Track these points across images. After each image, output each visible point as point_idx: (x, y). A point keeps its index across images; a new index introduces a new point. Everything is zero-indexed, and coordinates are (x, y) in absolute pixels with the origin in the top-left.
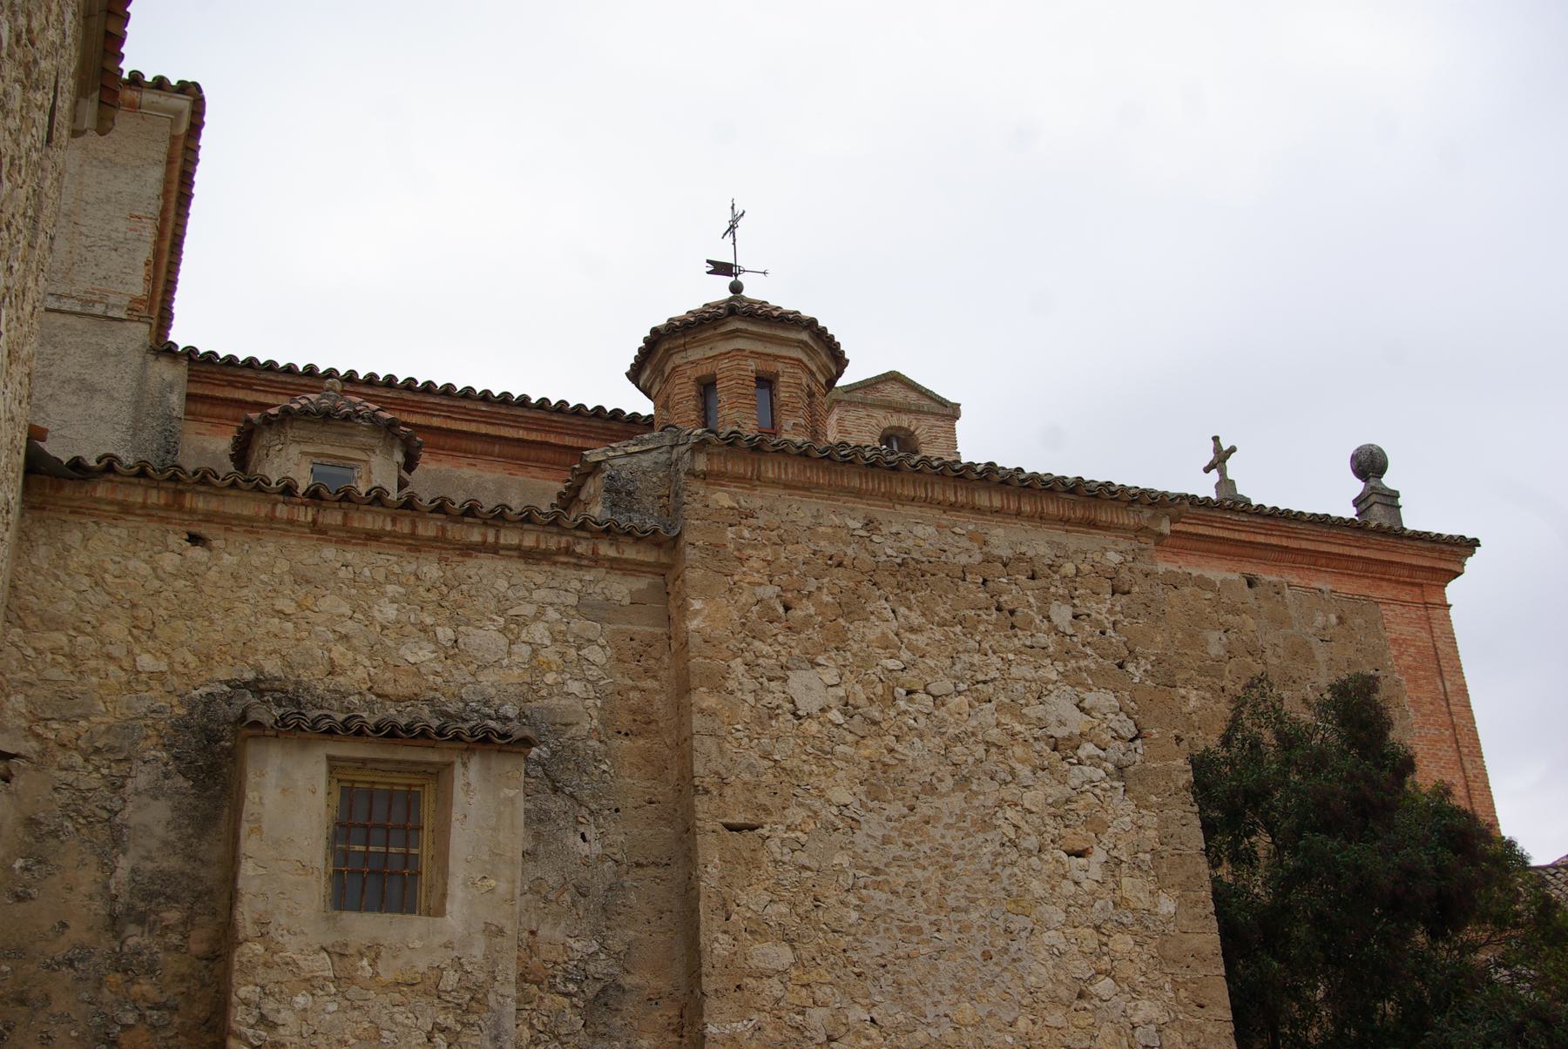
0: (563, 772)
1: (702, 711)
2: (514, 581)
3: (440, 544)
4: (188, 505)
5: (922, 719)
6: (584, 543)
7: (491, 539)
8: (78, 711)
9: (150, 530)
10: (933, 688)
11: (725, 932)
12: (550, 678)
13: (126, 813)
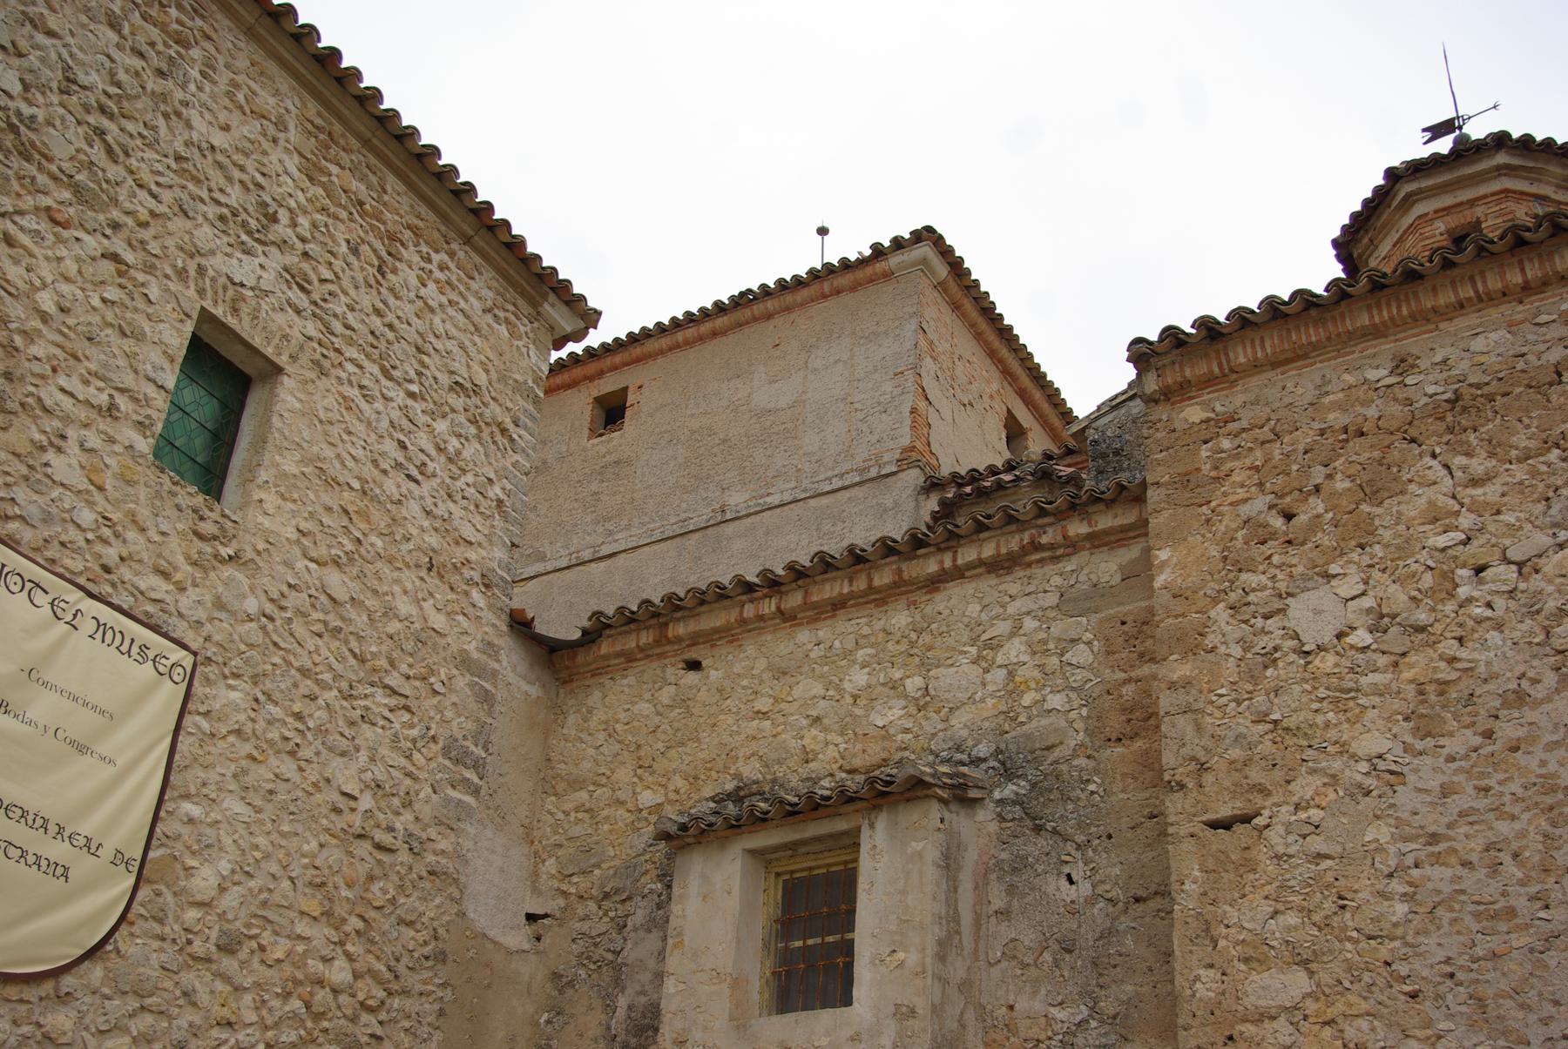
0: (1044, 805)
1: (1172, 686)
2: (985, 602)
3: (901, 589)
4: (670, 635)
5: (1500, 603)
6: (1050, 530)
7: (948, 563)
8: (593, 861)
9: (651, 669)
10: (1513, 554)
11: (1211, 966)
12: (1027, 700)
13: (625, 953)
